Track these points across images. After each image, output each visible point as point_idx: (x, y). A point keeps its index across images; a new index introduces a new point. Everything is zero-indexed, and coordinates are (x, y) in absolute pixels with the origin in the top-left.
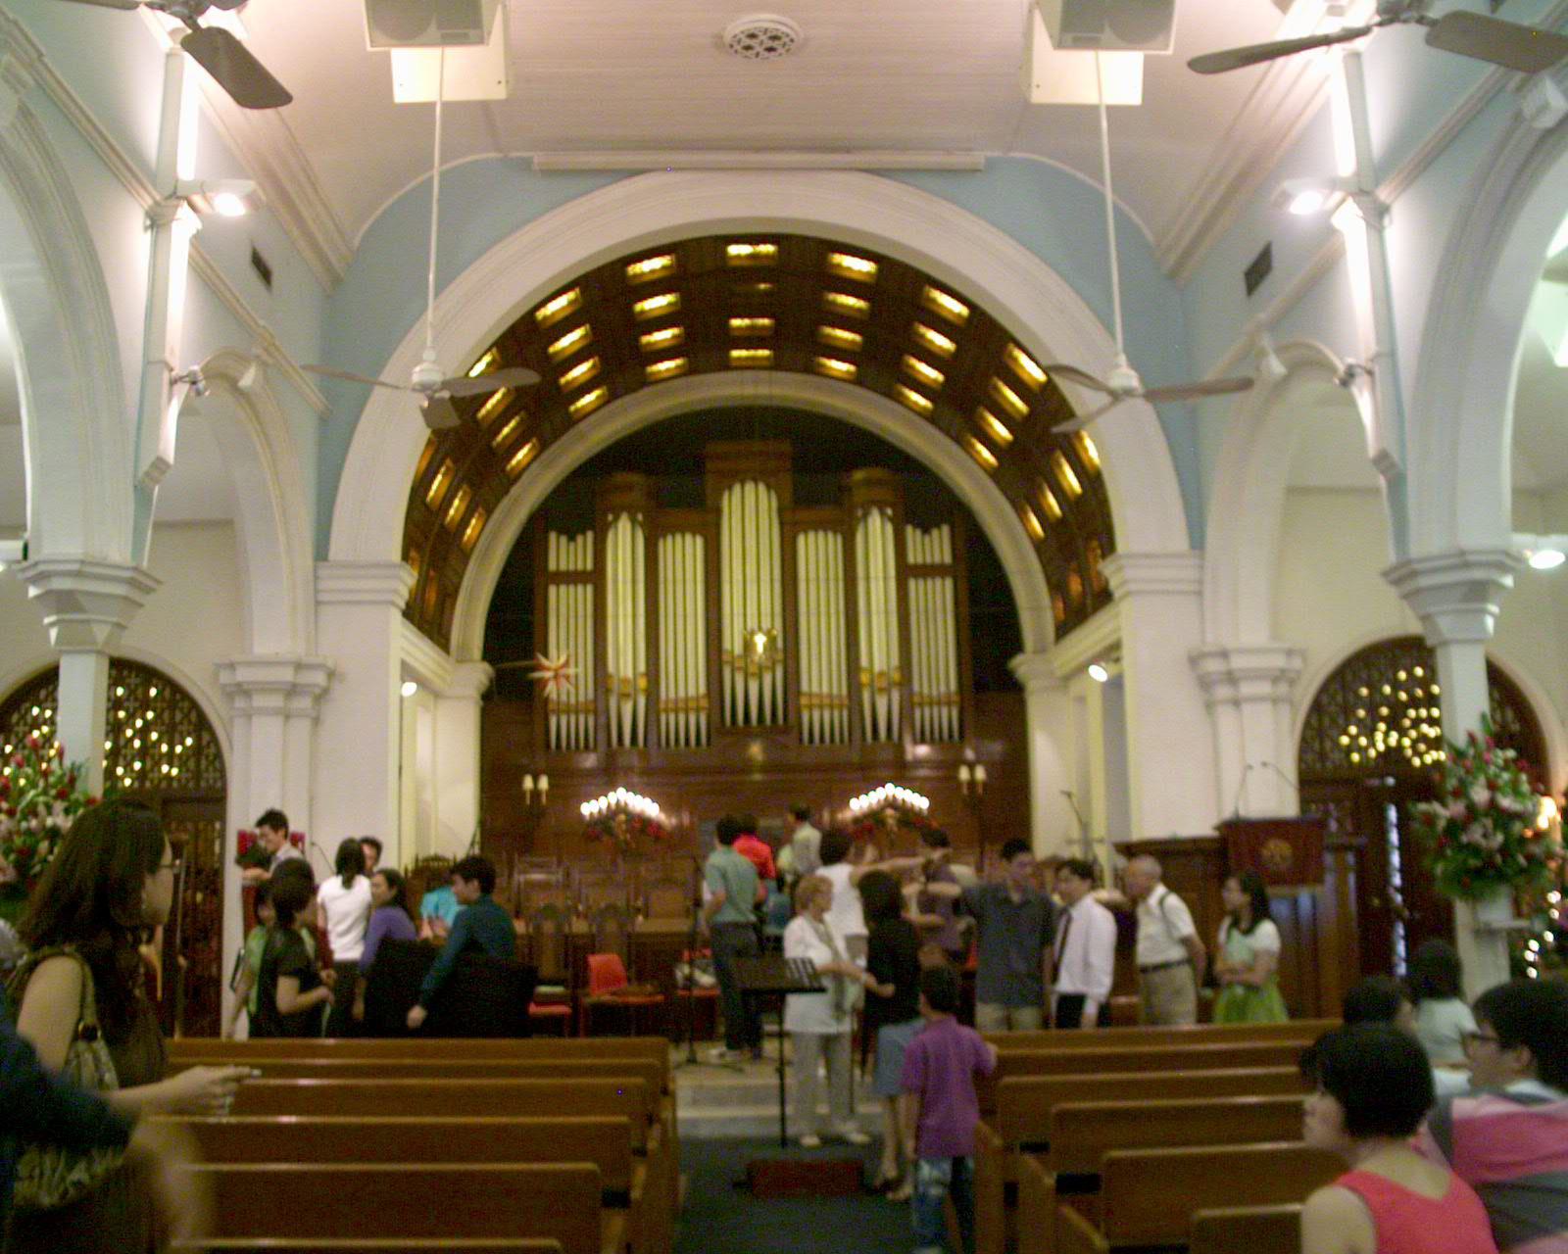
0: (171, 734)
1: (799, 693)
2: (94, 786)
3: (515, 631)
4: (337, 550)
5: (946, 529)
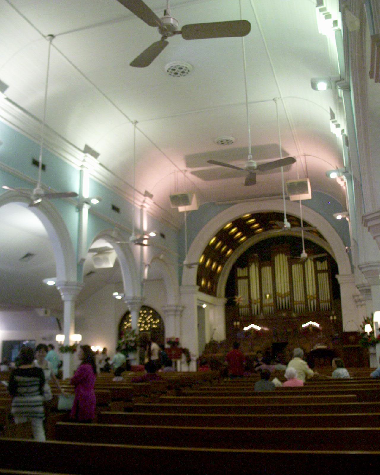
0: (155, 320)
1: (294, 301)
2: (137, 333)
3: (231, 290)
4: (184, 283)
5: (326, 262)
